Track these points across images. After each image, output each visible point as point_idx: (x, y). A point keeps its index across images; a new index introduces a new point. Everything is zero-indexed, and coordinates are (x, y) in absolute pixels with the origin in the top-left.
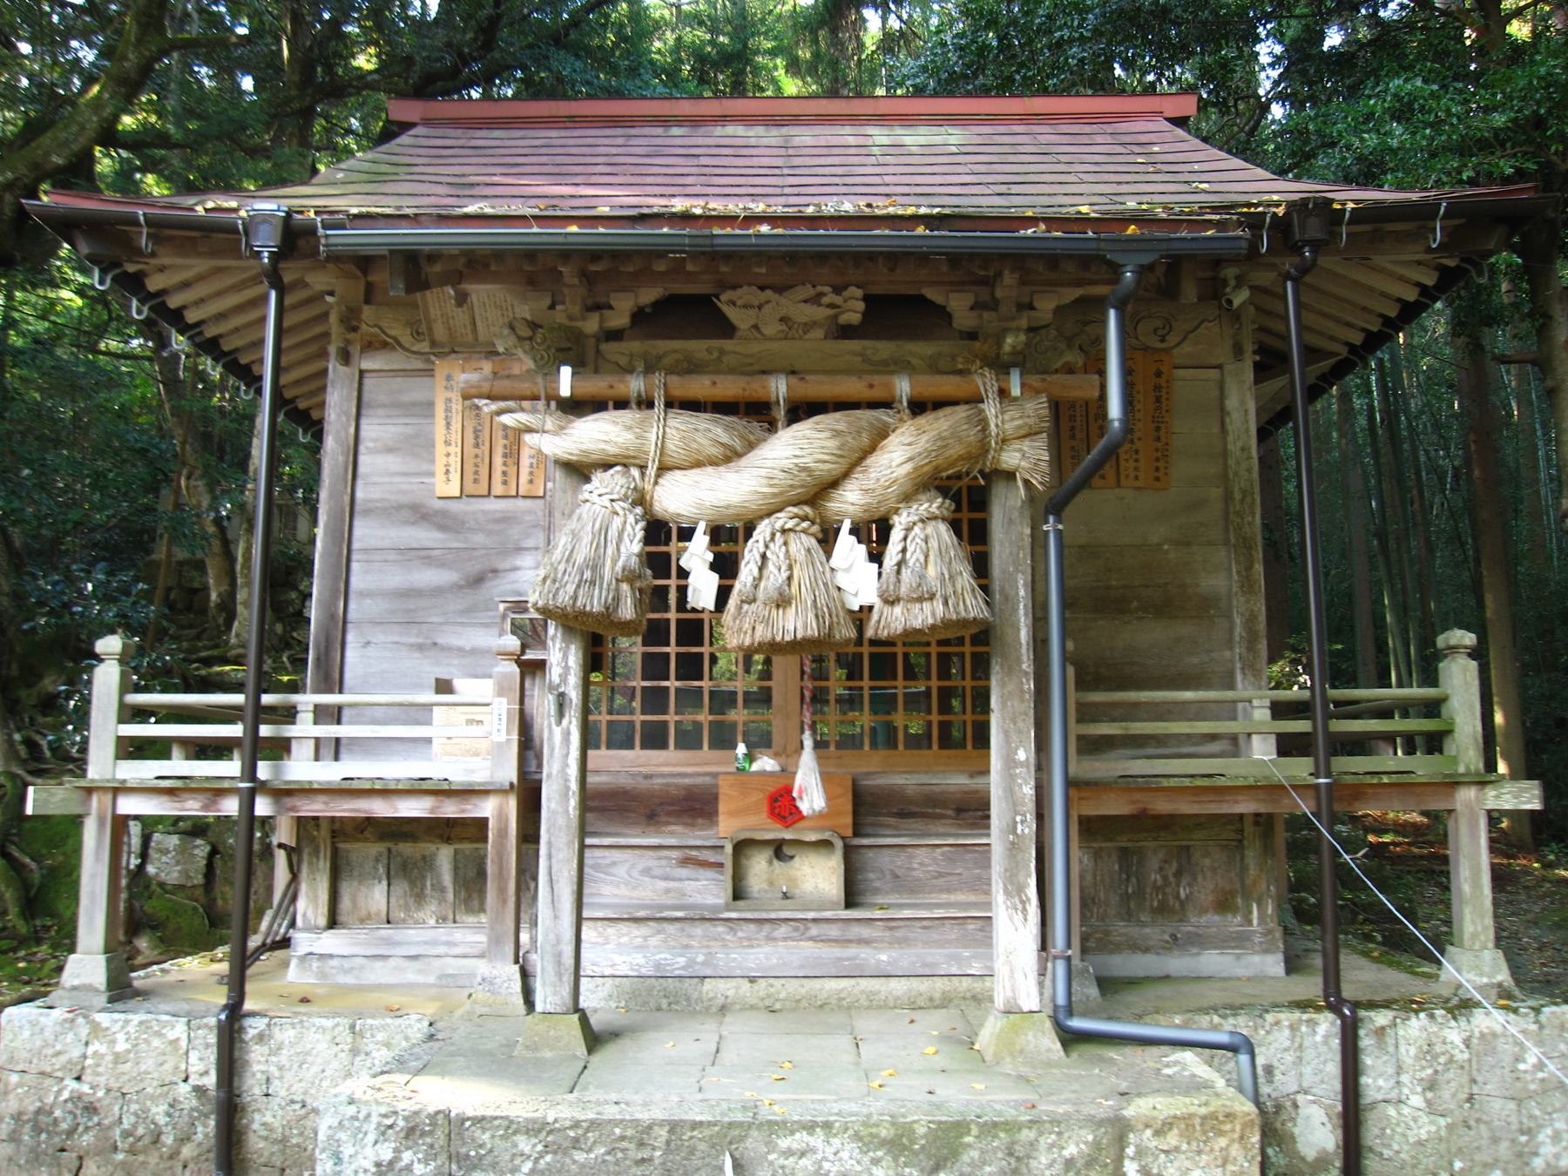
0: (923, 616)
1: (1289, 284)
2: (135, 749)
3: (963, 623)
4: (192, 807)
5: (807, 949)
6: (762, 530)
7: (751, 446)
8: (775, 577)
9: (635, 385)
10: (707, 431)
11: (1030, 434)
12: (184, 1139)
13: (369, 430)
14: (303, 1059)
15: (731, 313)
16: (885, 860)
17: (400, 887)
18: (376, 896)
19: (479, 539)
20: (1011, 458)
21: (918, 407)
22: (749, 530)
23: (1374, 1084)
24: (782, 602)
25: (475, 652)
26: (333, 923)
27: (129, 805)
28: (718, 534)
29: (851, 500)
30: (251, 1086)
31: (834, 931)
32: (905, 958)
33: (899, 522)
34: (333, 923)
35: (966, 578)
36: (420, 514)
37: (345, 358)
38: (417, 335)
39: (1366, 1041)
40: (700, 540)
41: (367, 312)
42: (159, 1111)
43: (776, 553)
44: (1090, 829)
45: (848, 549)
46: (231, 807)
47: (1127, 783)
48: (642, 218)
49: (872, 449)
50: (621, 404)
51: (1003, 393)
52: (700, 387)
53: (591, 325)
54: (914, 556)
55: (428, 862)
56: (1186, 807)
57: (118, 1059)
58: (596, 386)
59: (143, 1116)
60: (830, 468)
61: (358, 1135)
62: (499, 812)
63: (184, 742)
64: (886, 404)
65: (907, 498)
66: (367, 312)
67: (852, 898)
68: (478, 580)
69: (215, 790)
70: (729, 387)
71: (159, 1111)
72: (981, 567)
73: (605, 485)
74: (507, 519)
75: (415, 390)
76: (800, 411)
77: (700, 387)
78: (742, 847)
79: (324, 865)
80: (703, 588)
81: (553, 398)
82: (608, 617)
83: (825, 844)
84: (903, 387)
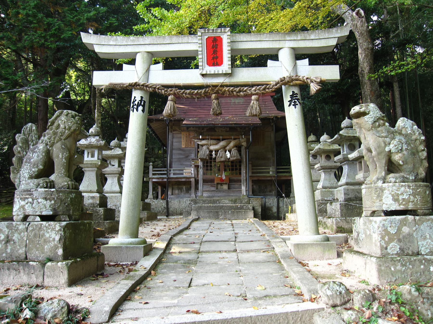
0: (234, 158)
1: (160, 188)
2: (153, 174)
3: (238, 159)
4: (160, 180)
5: (224, 194)
6: (220, 151)
7: (218, 143)
8: (221, 155)
9: (207, 137)
10: (214, 142)
11: (245, 142)
12: (163, 212)
13: (174, 140)
14: (174, 204)
15: (216, 130)
16: (232, 186)
17: (179, 191)
18: (177, 192)
19: (187, 152)
20: (243, 144)
21: (235, 139)
22: (218, 151)
23: (281, 205)
24: (222, 157)
25: (187, 165)
26: (172, 194)
27: (154, 180)
28: (215, 151)
29: (228, 148)
30: (169, 206)
31: (227, 192)
32: (234, 194)
33: (232, 150)
34: (172, 194)
35: (238, 155)
36: (180, 149)
37: (171, 132)
38: (179, 129)
39: (280, 201)
40: (214, 152)
41: (173, 127)
42: (160, 209)
43: (221, 153)
44: (253, 181)
45: (228, 153)
46: (165, 180)
47: (257, 176)
48: (209, 124)
49: (230, 143)
50: (206, 139)
51: (242, 138)
52: (213, 137)
53: (202, 131)
54: (234, 153)
55: (182, 188)
56: (263, 179)
57: (156, 204)
58: (204, 137)
59: (159, 209)
60: (225, 145)
61: (187, 201)
62: (193, 180)
63: (158, 173)
64: (231, 139)
65: (233, 148)
66: (173, 127)
67: (229, 189)
68: (187, 157)
69: (163, 178)
70: (216, 137)
71: (160, 209)
72: (240, 155)
73: (204, 147)
74: (190, 150)
75: (179, 135)
76: (223, 140)
77: (213, 137)
78: (218, 184)
79: (171, 188)
80: (214, 156)
81: (200, 139)
82: (206, 159)
83: (226, 184)
84: (233, 137)
